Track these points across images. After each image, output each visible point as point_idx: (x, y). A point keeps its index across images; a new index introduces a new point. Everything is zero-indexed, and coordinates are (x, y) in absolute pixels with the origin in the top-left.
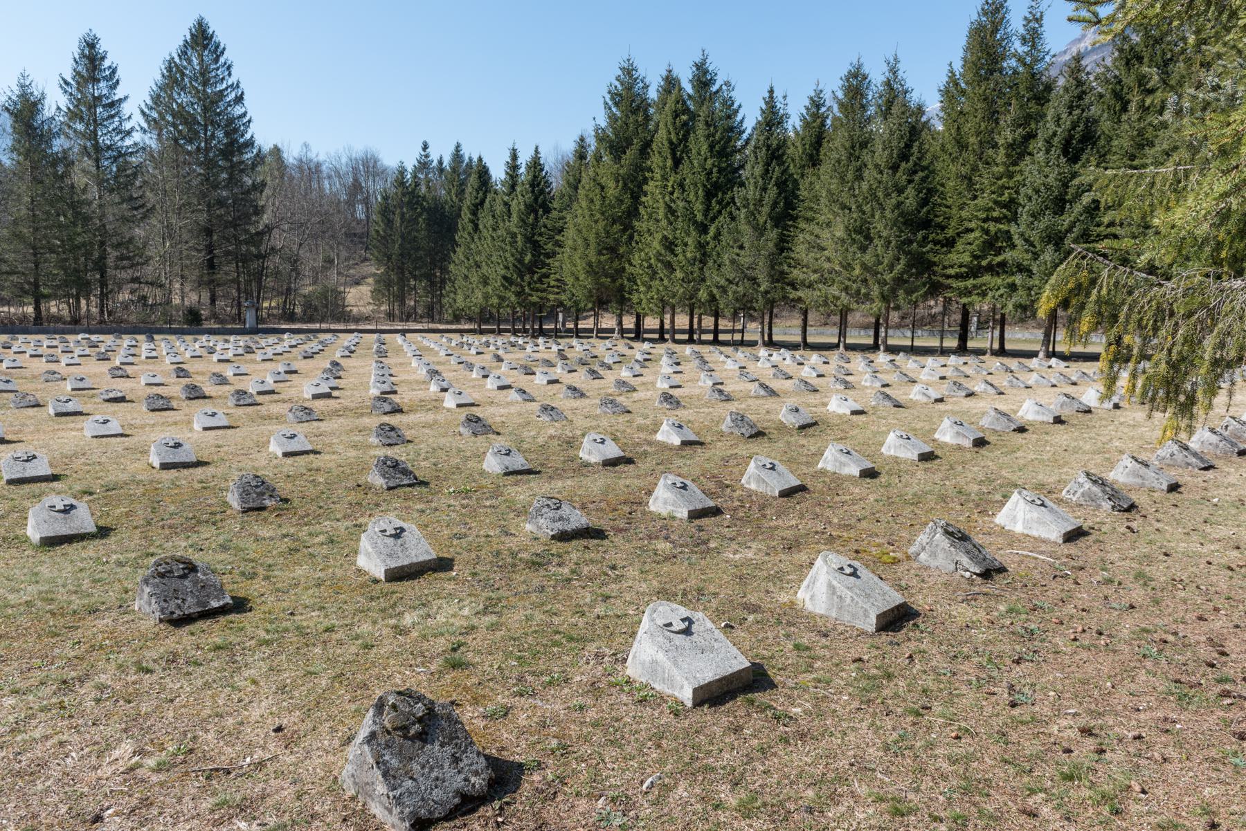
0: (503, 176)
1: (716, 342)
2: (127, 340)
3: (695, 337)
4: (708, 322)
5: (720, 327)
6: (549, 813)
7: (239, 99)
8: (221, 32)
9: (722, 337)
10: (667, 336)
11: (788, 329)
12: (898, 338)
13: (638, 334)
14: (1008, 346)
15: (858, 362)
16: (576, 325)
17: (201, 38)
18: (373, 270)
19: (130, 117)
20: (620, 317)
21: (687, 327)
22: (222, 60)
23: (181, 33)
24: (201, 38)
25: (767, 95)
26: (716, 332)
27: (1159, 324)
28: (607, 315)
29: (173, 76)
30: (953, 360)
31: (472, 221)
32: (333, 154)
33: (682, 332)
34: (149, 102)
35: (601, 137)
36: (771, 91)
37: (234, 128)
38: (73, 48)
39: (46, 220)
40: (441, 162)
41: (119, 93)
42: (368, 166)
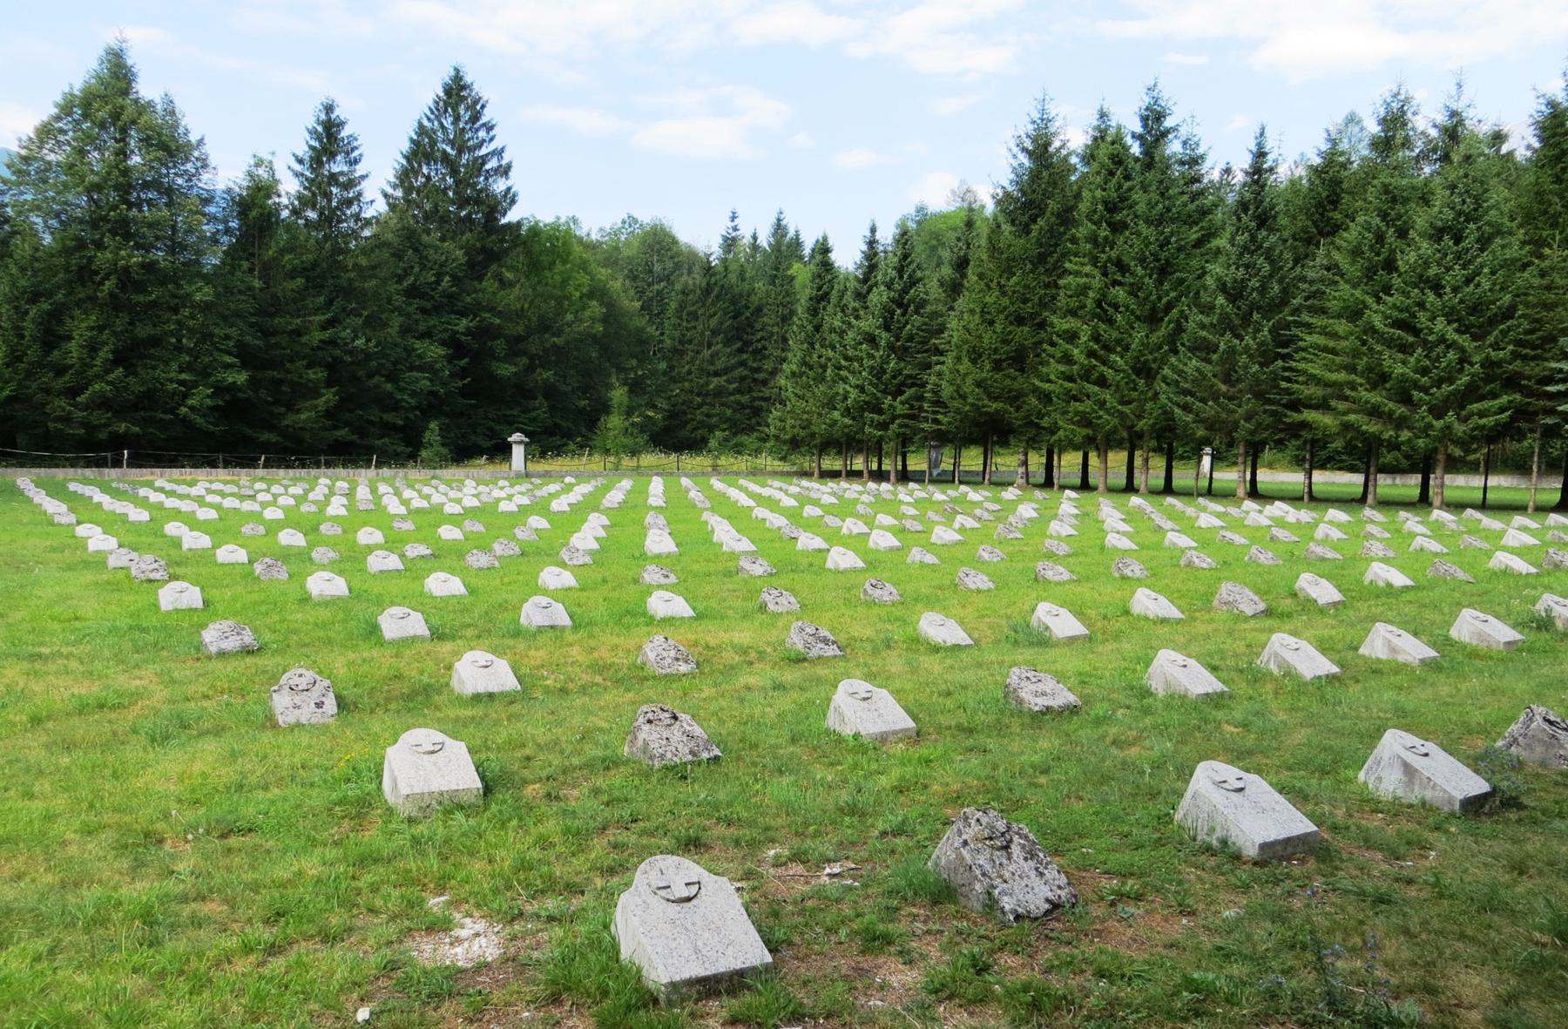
0: (890, 240)
6: (581, 779)
7: (505, 171)
8: (481, 84)
15: (1410, 521)
17: (456, 93)
19: (372, 202)
22: (484, 120)
23: (432, 90)
24: (456, 93)
25: (868, 234)
27: (469, 632)
29: (421, 150)
34: (393, 180)
35: (1004, 201)
36: (873, 230)
37: (493, 207)
38: (310, 118)
40: (755, 238)
41: (360, 170)
42: (659, 242)
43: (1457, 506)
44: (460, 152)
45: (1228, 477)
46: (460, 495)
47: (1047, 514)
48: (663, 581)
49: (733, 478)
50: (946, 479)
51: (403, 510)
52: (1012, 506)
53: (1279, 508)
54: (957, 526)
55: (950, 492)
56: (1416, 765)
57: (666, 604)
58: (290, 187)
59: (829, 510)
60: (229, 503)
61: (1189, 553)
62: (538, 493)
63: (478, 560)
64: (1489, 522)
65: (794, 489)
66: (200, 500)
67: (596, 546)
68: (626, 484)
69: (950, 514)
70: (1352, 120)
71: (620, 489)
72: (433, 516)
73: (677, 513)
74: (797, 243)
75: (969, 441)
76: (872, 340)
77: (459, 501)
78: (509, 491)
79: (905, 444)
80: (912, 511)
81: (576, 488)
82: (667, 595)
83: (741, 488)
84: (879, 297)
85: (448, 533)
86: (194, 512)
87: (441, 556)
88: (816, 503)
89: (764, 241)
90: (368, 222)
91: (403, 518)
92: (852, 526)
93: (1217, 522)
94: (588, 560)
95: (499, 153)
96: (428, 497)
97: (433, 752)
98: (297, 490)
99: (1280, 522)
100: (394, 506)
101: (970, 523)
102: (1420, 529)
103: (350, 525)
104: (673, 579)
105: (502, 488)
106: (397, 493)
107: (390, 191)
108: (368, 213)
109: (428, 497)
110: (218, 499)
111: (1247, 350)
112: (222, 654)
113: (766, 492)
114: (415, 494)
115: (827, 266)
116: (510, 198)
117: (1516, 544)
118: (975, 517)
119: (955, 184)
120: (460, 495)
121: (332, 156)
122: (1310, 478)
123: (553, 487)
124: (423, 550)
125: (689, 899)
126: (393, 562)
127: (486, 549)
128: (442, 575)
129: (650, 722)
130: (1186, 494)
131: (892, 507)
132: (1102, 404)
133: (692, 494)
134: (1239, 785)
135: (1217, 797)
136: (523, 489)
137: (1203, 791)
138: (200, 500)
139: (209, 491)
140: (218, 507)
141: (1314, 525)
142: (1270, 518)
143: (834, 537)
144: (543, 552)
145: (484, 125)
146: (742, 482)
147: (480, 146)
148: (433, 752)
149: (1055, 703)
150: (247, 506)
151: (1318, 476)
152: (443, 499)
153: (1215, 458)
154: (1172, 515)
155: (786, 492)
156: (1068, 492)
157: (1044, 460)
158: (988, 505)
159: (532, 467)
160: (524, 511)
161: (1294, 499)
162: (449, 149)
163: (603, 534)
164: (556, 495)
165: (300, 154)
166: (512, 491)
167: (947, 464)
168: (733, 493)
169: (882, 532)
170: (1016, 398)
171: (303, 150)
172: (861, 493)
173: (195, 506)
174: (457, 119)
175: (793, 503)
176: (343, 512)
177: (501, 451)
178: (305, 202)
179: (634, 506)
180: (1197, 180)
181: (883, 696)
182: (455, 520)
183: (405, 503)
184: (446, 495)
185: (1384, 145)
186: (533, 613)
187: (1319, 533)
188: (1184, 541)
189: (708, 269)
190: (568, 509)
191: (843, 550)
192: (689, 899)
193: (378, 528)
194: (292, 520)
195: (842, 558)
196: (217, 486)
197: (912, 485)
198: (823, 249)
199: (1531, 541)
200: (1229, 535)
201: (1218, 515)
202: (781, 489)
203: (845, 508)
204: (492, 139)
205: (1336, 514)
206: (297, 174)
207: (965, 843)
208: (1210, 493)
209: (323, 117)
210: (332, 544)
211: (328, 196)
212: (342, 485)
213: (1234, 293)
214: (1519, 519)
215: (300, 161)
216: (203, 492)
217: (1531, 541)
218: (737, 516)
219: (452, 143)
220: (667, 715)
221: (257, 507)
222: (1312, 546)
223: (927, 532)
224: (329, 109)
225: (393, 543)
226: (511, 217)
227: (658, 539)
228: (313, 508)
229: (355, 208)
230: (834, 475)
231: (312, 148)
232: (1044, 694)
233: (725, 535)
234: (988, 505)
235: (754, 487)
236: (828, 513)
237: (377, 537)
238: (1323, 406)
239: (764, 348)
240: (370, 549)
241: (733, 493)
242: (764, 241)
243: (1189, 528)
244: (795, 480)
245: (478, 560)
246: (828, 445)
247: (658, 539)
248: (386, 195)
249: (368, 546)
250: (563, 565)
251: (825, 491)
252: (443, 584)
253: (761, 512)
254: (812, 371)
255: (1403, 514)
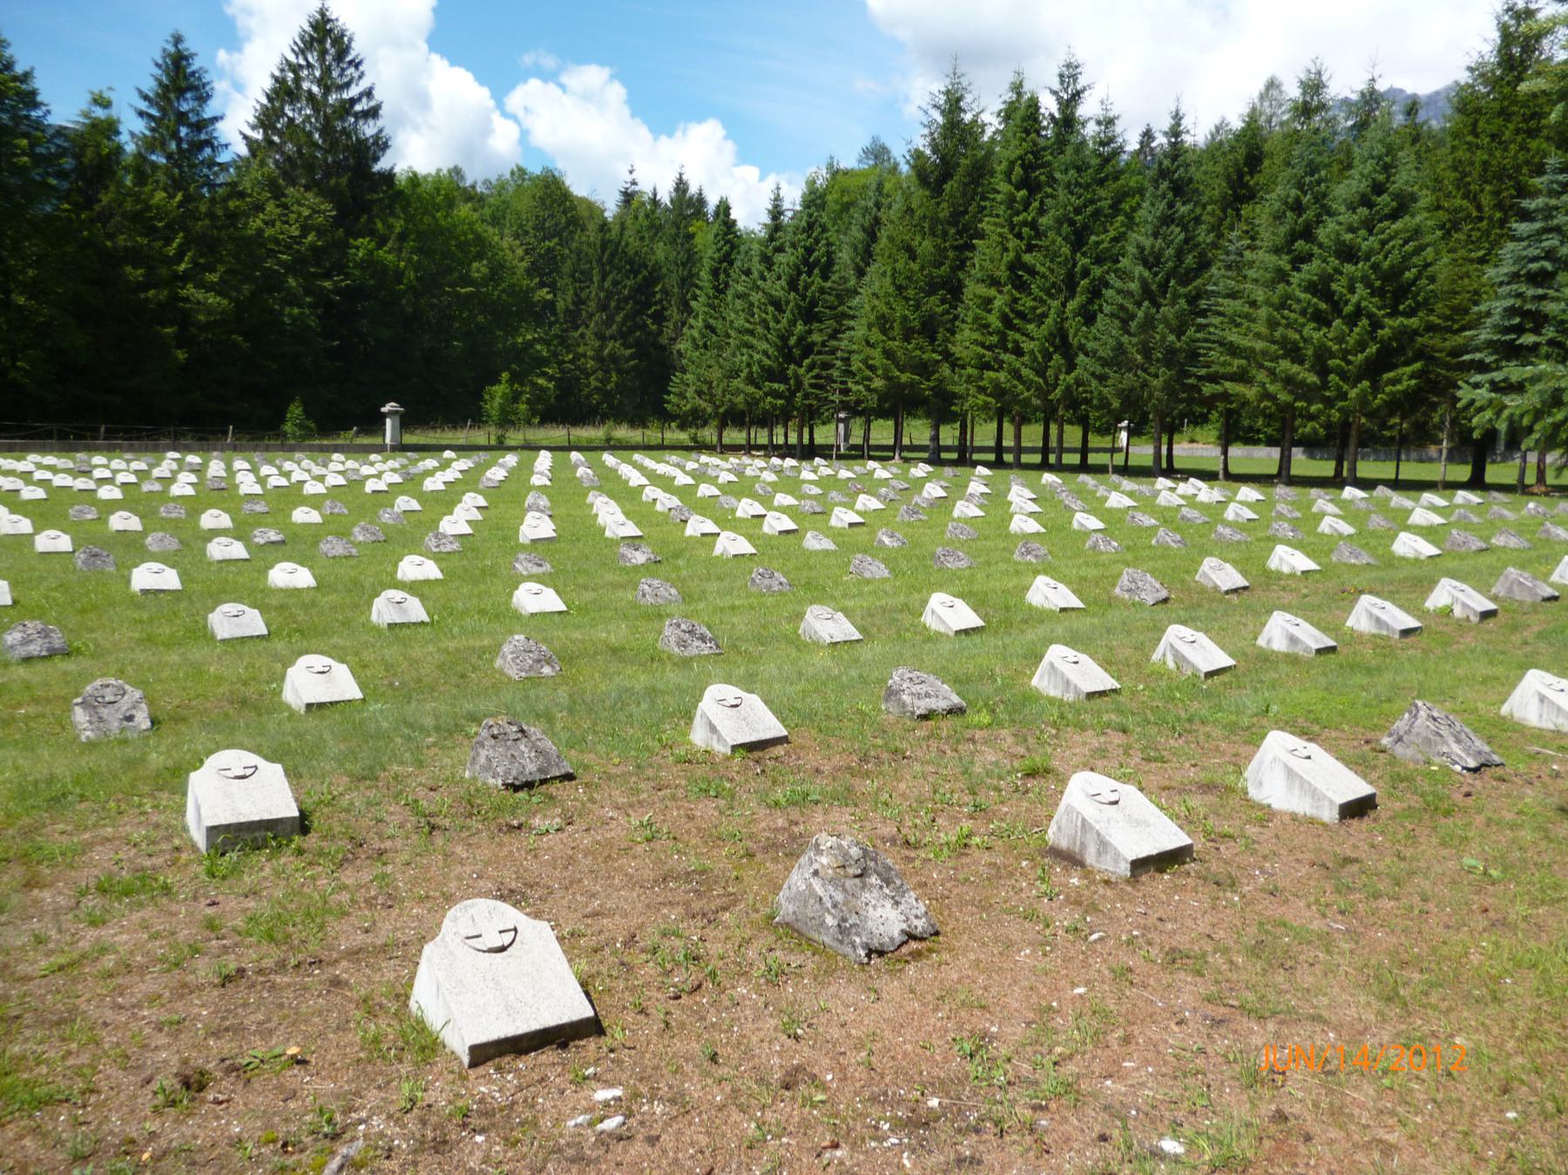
1: (1084, 468)
2: (978, 481)
3: (1052, 459)
4: (1073, 435)
5: (1090, 445)
7: (373, 113)
9: (1093, 459)
10: (1008, 458)
11: (1196, 448)
12: (1366, 469)
13: (964, 457)
14: (1177, 465)
15: (1321, 501)
16: (898, 435)
18: (199, 295)
20: (936, 428)
21: (1040, 444)
26: (1084, 450)
28: (918, 423)
30: (1462, 496)
31: (1095, 352)
32: (494, 181)
33: (1032, 450)
36: (140, 92)
39: (801, 339)
43: (1367, 485)
44: (327, 90)
45: (1143, 453)
46: (323, 471)
47: (957, 491)
48: (536, 570)
49: (626, 453)
50: (859, 453)
51: (258, 489)
52: (919, 484)
53: (1193, 486)
54: (859, 506)
55: (857, 468)
56: (1296, 769)
57: (535, 598)
58: (132, 128)
59: (728, 489)
60: (60, 480)
61: (1094, 537)
62: (412, 470)
63: (333, 547)
64: (1398, 499)
65: (691, 465)
66: (26, 476)
67: (467, 530)
68: (511, 459)
69: (850, 493)
70: (1272, 85)
71: (502, 466)
72: (292, 495)
73: (565, 496)
74: (701, 201)
75: (882, 414)
76: (778, 305)
77: (321, 479)
78: (380, 467)
79: (811, 416)
80: (816, 490)
81: (454, 464)
82: (535, 586)
83: (635, 465)
84: (785, 260)
85: (303, 515)
86: (17, 491)
87: (296, 545)
88: (713, 481)
89: (665, 197)
90: (224, 167)
91: (633, 542)
92: (747, 508)
93: (1128, 502)
94: (456, 546)
95: (368, 93)
96: (287, 475)
97: (243, 777)
98: (141, 465)
99: (1191, 500)
100: (247, 484)
101: (874, 504)
102: (1331, 508)
103: (195, 506)
104: (547, 567)
105: (372, 464)
106: (254, 470)
107: (249, 132)
108: (223, 157)
109: (287, 475)
110: (48, 475)
111: (1165, 320)
112: (27, 660)
113: (662, 468)
114: (274, 471)
115: (730, 225)
116: (381, 144)
117: (1424, 523)
118: (878, 496)
119: (866, 142)
120: (323, 471)
121: (181, 92)
122: (1225, 453)
123: (430, 463)
124: (273, 536)
125: (502, 949)
126: (238, 550)
127: (343, 534)
128: (289, 566)
129: (494, 737)
130: (1100, 470)
131: (791, 484)
132: (1016, 374)
133: (581, 471)
134: (1114, 797)
135: (1090, 812)
136: (397, 465)
137: (1075, 804)
138: (26, 476)
139: (39, 466)
140: (43, 483)
141: (1223, 504)
142: (1182, 497)
143: (727, 521)
144: (413, 533)
145: (350, 62)
146: (637, 456)
147: (347, 85)
148: (243, 777)
149: (941, 704)
150: (81, 483)
151: (1236, 451)
152: (306, 476)
153: (1132, 433)
154: (1080, 493)
155: (682, 468)
156: (979, 468)
157: (957, 433)
158: (894, 483)
159: (409, 439)
160: (394, 490)
161: (1207, 476)
162: (315, 89)
163: (477, 516)
164: (430, 473)
165: (145, 90)
166: (385, 467)
167: (857, 439)
168: (626, 471)
169: (778, 514)
170: (924, 369)
171: (149, 86)
172: (762, 469)
173: (18, 484)
174: (323, 53)
175: (689, 480)
176: (190, 491)
177: (373, 423)
178: (151, 144)
179: (517, 485)
180: (1111, 140)
181: (754, 702)
182: (315, 502)
183: (262, 481)
184: (309, 471)
185: (1305, 110)
186: (386, 609)
187: (1230, 513)
188: (1093, 523)
189: (604, 226)
190: (443, 487)
191: (732, 535)
192: (502, 949)
193: (226, 510)
194: (132, 499)
195: (732, 544)
196: (50, 460)
197: (817, 460)
198: (724, 208)
199: (1437, 520)
200: (1139, 516)
201: (1131, 494)
202: (677, 465)
203: (742, 487)
204: (360, 77)
205: (1248, 493)
206: (141, 114)
207: (816, 873)
208: (1126, 471)
209: (172, 49)
210: (173, 526)
211: (175, 135)
212: (193, 459)
213: (1150, 260)
214: (1428, 497)
215: (146, 97)
216: (31, 467)
217: (1437, 520)
218: (627, 497)
219: (319, 82)
220: (515, 729)
221: (91, 485)
222: (1220, 529)
223: (825, 513)
224: (178, 40)
225: (239, 532)
226: (382, 165)
227: (535, 522)
228: (157, 487)
229: (208, 151)
230: (735, 449)
231: (161, 84)
232: (928, 695)
233: (611, 518)
234: (894, 483)
235: (649, 463)
236: (725, 493)
237: (225, 521)
238: (1242, 377)
239: (664, 309)
240: (215, 533)
241: (626, 471)
242: (665, 197)
243: (1096, 506)
244: (694, 455)
245: (333, 547)
246: (734, 417)
247: (535, 522)
248: (245, 137)
249: (211, 530)
250: (428, 554)
251: (723, 468)
252: (289, 575)
253: (651, 492)
254: (712, 337)
255: (1314, 492)
